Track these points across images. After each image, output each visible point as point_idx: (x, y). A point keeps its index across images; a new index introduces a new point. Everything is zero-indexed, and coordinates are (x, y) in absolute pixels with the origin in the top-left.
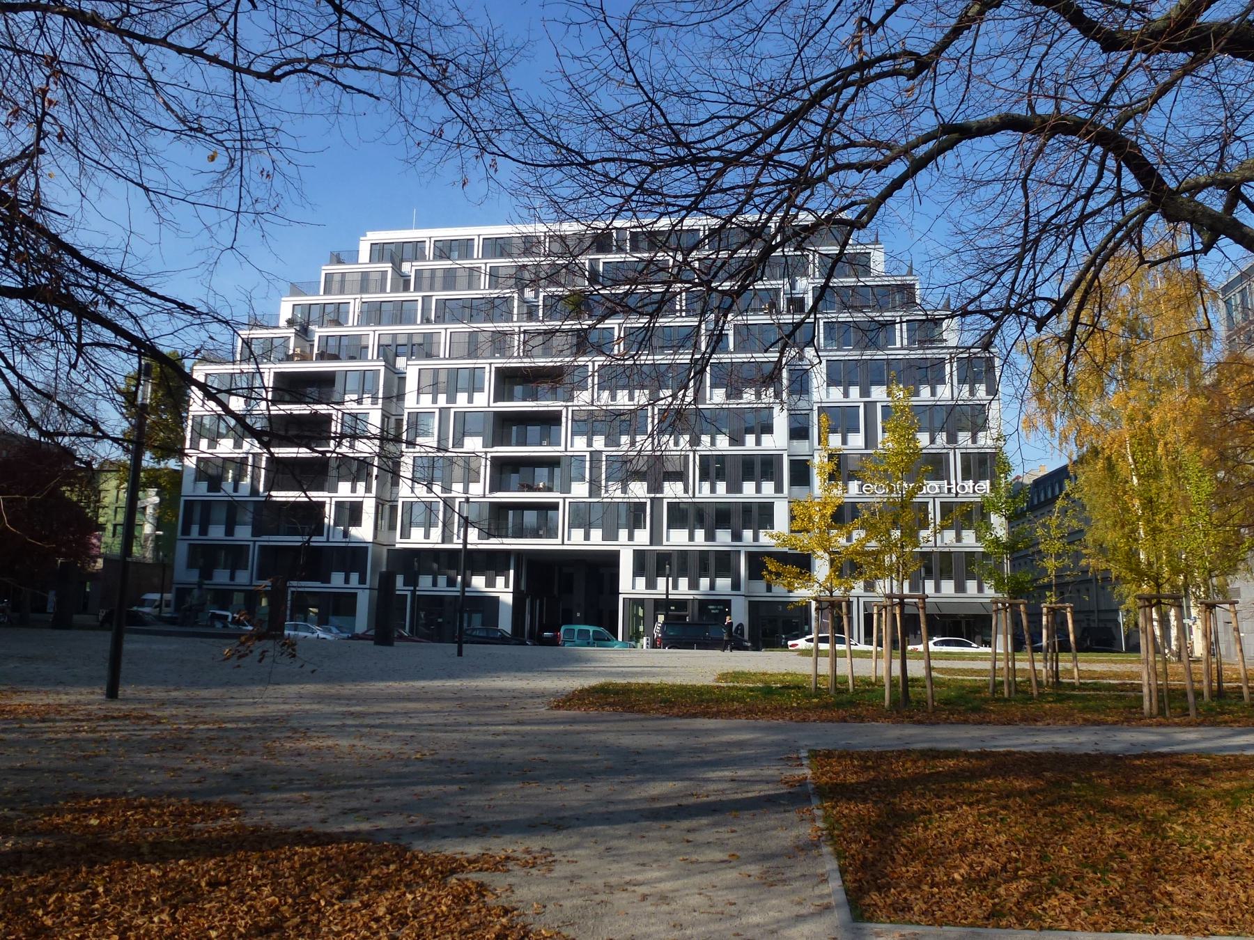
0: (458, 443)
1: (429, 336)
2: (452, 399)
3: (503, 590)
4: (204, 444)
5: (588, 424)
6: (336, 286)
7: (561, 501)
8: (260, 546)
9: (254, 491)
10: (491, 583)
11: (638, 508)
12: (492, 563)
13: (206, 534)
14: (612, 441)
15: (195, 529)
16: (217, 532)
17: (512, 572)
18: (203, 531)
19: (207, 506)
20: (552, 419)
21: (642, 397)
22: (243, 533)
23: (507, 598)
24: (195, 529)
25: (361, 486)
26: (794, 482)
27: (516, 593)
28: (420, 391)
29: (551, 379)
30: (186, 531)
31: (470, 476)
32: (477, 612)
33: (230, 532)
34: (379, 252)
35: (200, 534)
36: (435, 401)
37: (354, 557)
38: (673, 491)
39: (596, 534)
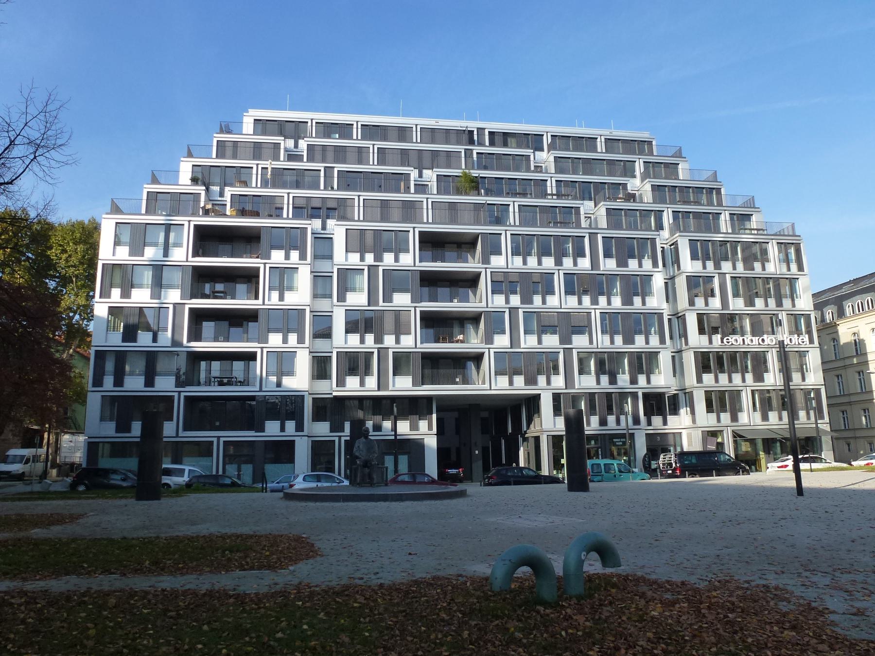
0: (388, 298)
1: (342, 202)
2: (378, 258)
3: (426, 432)
4: (116, 293)
5: (503, 284)
6: (229, 151)
7: (259, 351)
8: (186, 397)
9: (176, 343)
10: (414, 427)
11: (552, 357)
12: (413, 407)
13: (152, 385)
14: (527, 299)
15: (109, 382)
16: (134, 384)
17: (434, 416)
18: (119, 381)
19: (121, 357)
20: (472, 281)
21: (549, 262)
22: (165, 384)
23: (431, 442)
24: (109, 382)
25: (293, 338)
26: (316, 336)
27: (440, 433)
28: (117, 243)
29: (464, 245)
30: (98, 381)
31: (399, 330)
32: (404, 454)
33: (150, 382)
34: (261, 125)
35: (115, 385)
36: (362, 259)
37: (288, 407)
38: (580, 341)
39: (519, 381)
